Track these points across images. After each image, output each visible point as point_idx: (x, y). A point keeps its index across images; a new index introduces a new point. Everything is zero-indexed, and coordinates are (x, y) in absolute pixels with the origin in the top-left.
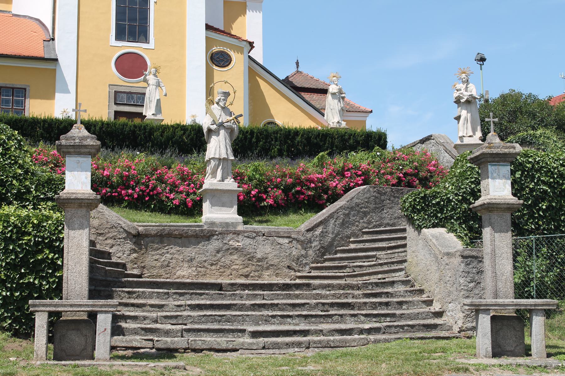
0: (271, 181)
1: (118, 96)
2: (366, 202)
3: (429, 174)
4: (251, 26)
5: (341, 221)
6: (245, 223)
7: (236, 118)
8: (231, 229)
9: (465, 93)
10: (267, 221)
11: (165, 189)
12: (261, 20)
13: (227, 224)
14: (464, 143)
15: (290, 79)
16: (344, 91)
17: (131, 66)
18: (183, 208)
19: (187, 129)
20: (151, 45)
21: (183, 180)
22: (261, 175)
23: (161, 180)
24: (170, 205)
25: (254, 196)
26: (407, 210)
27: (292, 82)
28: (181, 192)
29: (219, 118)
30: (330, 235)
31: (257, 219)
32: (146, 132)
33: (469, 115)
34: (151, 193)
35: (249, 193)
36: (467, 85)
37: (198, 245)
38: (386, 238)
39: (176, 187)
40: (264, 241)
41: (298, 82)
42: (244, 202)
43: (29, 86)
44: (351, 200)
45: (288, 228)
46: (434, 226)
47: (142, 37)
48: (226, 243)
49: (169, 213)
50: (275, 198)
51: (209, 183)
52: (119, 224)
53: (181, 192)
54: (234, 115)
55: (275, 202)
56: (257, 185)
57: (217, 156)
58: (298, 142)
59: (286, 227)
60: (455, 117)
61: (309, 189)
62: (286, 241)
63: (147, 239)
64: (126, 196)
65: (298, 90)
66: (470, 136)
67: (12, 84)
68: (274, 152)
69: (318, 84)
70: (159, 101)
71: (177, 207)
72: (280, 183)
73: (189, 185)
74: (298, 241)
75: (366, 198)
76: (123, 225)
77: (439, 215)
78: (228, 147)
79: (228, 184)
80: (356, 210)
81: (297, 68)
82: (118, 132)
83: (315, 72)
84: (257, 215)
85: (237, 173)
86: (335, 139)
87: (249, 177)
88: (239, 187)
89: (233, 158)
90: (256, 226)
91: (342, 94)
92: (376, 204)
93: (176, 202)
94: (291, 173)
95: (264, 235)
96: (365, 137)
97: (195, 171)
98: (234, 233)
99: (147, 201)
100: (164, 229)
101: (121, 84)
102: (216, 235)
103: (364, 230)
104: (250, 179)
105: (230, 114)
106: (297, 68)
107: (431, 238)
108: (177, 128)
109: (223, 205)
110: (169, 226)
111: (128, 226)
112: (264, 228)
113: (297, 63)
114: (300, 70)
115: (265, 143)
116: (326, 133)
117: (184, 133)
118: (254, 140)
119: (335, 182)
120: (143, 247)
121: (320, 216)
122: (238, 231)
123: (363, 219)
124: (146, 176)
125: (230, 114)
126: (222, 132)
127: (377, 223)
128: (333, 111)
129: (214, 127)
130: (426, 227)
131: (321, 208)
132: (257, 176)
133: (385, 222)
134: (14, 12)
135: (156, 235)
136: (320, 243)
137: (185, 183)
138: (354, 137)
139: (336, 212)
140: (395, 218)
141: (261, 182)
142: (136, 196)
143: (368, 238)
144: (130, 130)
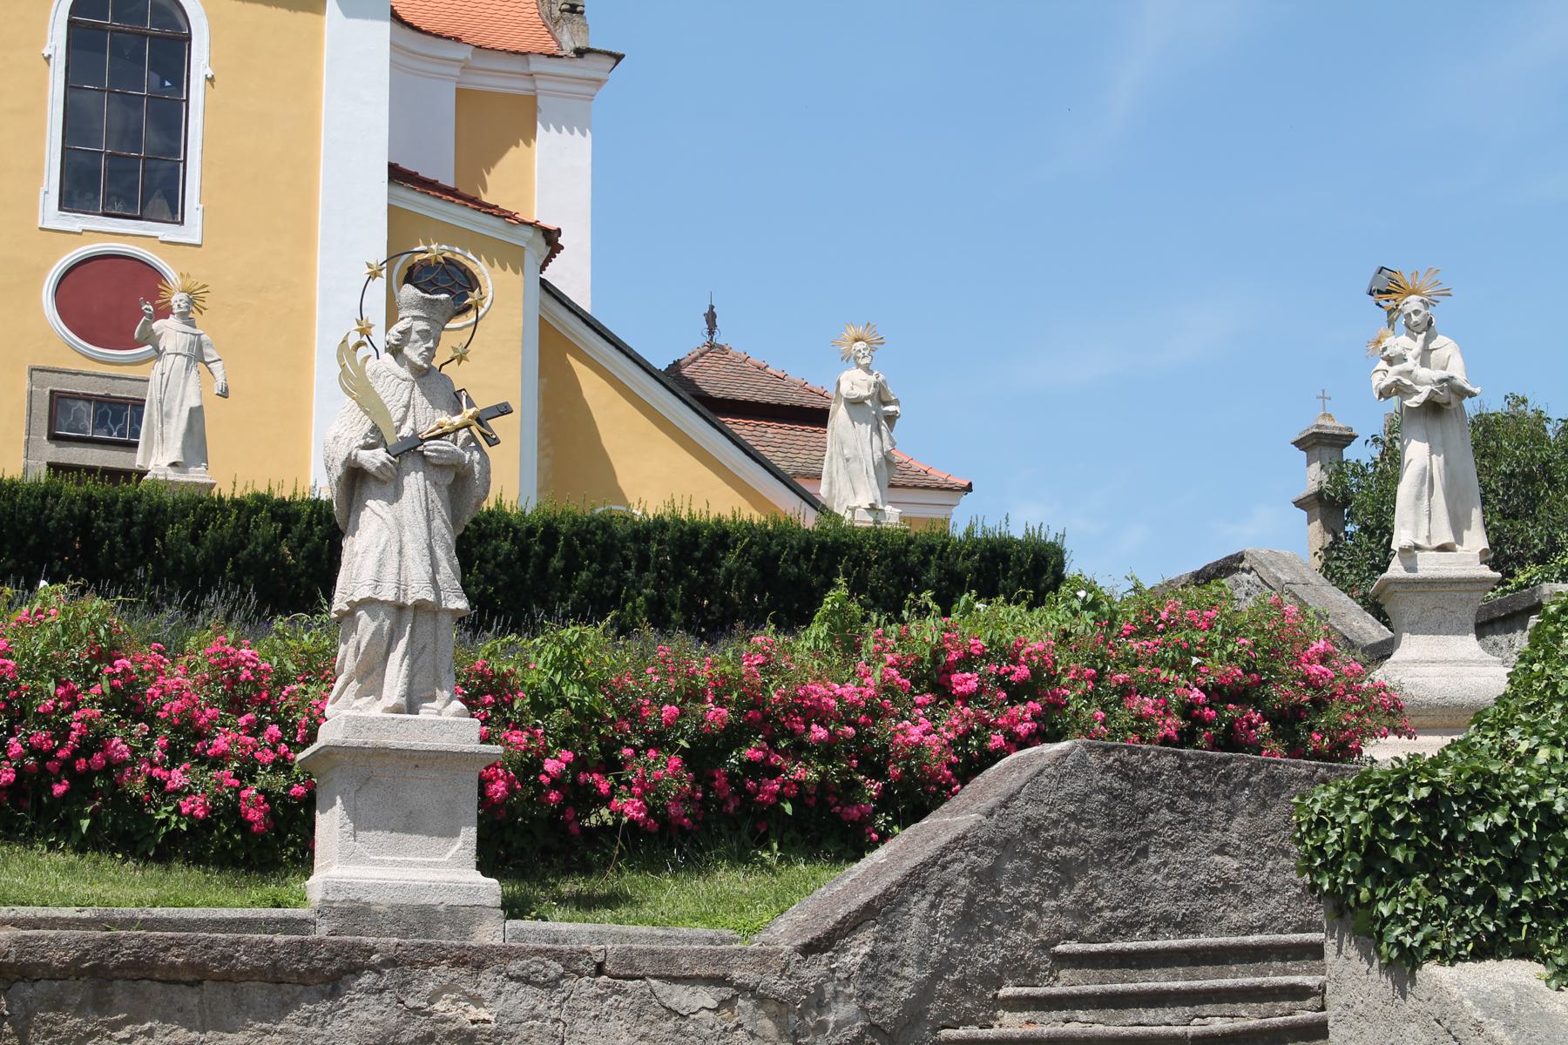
0: (634, 715)
1: (62, 412)
2: (1072, 816)
3: (1309, 693)
4: (551, 173)
5: (959, 902)
6: (513, 908)
7: (479, 420)
8: (446, 938)
9: (1422, 373)
10: (612, 901)
11: (147, 746)
12: (589, 160)
13: (426, 917)
14: (1422, 573)
15: (685, 372)
16: (892, 391)
17: (107, 300)
18: (229, 834)
19: (297, 516)
21: (236, 705)
22: (589, 685)
23: (128, 702)
24: (165, 822)
25: (556, 782)
26: (1333, 865)
27: (692, 381)
28: (217, 762)
29: (403, 420)
30: (908, 971)
31: (567, 887)
32: (133, 524)
33: (1438, 461)
34: (81, 764)
35: (530, 767)
36: (1427, 341)
37: (280, 1020)
38: (1178, 992)
39: (199, 735)
40: (603, 998)
41: (715, 382)
42: (512, 810)
44: (1004, 805)
45: (710, 933)
46: (1485, 950)
47: (158, 202)
48: (417, 1010)
49: (163, 856)
50: (649, 789)
51: (349, 716)
53: (217, 762)
54: (471, 404)
55: (651, 811)
56: (569, 730)
57: (388, 594)
58: (730, 573)
59: (701, 930)
60: (1296, 498)
61: (800, 749)
62: (706, 997)
63: (27, 991)
65: (715, 408)
66: (1442, 548)
68: (634, 609)
69: (781, 388)
70: (196, 415)
71: (201, 828)
72: (673, 725)
73: (256, 729)
74: (761, 1000)
75: (1070, 798)
77: (1506, 893)
78: (440, 553)
79: (434, 724)
80: (1026, 854)
81: (711, 333)
82: (23, 522)
83: (773, 348)
84: (568, 871)
85: (482, 676)
86: (869, 565)
87: (535, 694)
88: (485, 739)
89: (462, 604)
90: (565, 927)
91: (886, 404)
92: (1112, 825)
93: (197, 805)
94: (724, 676)
95: (600, 969)
96: (982, 558)
97: (291, 667)
98: (459, 962)
100: (113, 940)
101: (74, 368)
102: (372, 968)
103: (1060, 948)
104: (541, 706)
105: (455, 401)
106: (711, 333)
107: (1478, 1014)
108: (257, 510)
109: (410, 823)
110: (148, 924)
112: (599, 937)
113: (711, 318)
114: (719, 339)
115: (601, 574)
116: (836, 540)
117: (285, 532)
118: (556, 562)
119: (915, 723)
120: (7, 1028)
121: (860, 882)
122: (479, 950)
123: (1055, 895)
124: (59, 683)
125: (455, 401)
126: (414, 482)
127: (1120, 913)
128: (854, 466)
129: (375, 458)
130: (1446, 956)
131: (851, 842)
132: (572, 691)
133: (1156, 907)
135: (72, 971)
136: (863, 1009)
137: (242, 721)
138: (940, 558)
139: (938, 861)
140: (1197, 894)
141: (587, 717)
143: (1091, 988)
144: (71, 515)
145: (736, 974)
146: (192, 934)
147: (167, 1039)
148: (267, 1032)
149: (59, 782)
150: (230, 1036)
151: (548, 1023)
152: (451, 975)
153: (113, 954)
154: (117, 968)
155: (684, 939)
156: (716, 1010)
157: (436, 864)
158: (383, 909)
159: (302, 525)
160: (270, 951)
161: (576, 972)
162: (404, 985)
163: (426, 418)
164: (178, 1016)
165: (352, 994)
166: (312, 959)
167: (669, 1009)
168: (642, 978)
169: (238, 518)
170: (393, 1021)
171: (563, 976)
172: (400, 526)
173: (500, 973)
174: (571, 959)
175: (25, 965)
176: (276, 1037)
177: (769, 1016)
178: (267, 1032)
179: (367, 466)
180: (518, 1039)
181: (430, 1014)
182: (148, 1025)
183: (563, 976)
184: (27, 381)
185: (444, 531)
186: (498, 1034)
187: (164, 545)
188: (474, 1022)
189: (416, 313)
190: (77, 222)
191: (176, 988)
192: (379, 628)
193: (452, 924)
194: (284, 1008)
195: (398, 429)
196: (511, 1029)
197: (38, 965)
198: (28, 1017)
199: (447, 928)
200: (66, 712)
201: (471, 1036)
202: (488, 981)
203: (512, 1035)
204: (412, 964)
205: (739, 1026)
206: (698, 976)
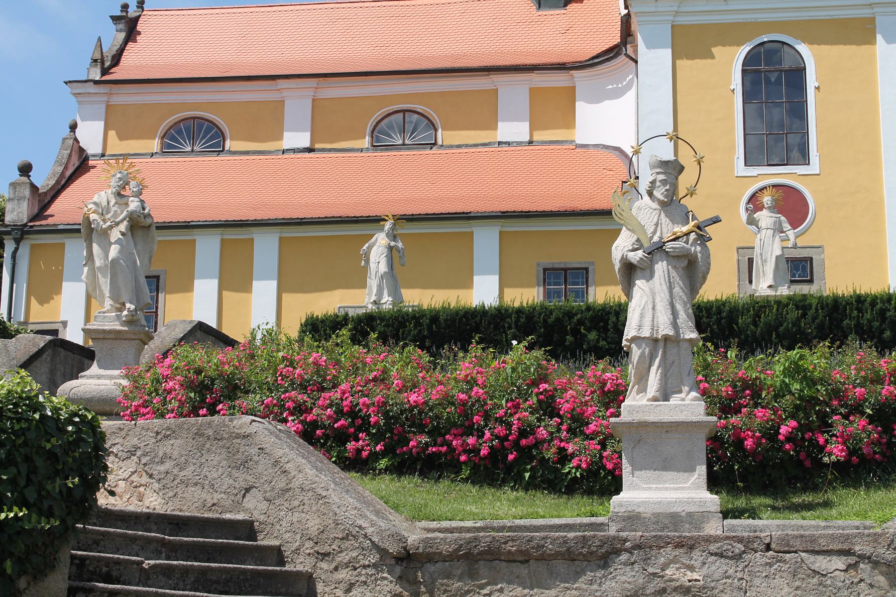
6: (726, 514)
10: (827, 504)
11: (559, 430)
13: (675, 519)
20: (814, 167)
25: (789, 439)
29: (654, 232)
32: (722, 318)
37: (575, 581)
40: (771, 565)
43: (593, 263)
48: (654, 574)
51: (638, 405)
52: (360, 527)
57: (646, 333)
59: (857, 522)
62: (839, 563)
63: (431, 568)
64: (465, 451)
67: (565, 263)
74: (876, 564)
76: (370, 531)
78: (679, 307)
79: (676, 406)
88: (708, 414)
89: (694, 335)
95: (768, 548)
98: (679, 545)
99: (511, 464)
100: (475, 539)
102: (626, 550)
109: (666, 465)
111: (380, 532)
120: (423, 589)
134: (578, 142)
135: (453, 557)
142: (484, 452)
145: (857, 548)
146: (520, 534)
147: (511, 594)
148: (568, 589)
149: (512, 453)
150: (547, 591)
151: (736, 581)
152: (674, 554)
153: (476, 546)
154: (479, 554)
155: (839, 528)
156: (846, 571)
157: (682, 488)
158: (648, 515)
159: (813, 311)
160: (565, 542)
161: (752, 549)
162: (646, 560)
163: (669, 229)
164: (517, 580)
165: (615, 566)
166: (590, 546)
167: (814, 571)
168: (796, 552)
169: (777, 310)
170: (641, 581)
171: (744, 552)
172: (653, 294)
173: (704, 551)
174: (749, 542)
175: (428, 554)
176: (573, 592)
177: (882, 573)
178: (568, 589)
179: (634, 262)
180: (717, 591)
181: (663, 577)
182: (499, 586)
183: (744, 552)
184: (736, 254)
185: (681, 294)
186: (704, 588)
187: (738, 327)
188: (690, 581)
189: (658, 170)
190: (754, 171)
191: (514, 564)
192: (643, 353)
193: (691, 523)
194: (578, 575)
195: (652, 238)
196: (713, 584)
197: (435, 553)
198: (433, 583)
199: (687, 526)
200: (511, 415)
201: (688, 590)
202: (697, 556)
203: (713, 588)
204: (650, 547)
205: (862, 580)
206: (832, 550)
